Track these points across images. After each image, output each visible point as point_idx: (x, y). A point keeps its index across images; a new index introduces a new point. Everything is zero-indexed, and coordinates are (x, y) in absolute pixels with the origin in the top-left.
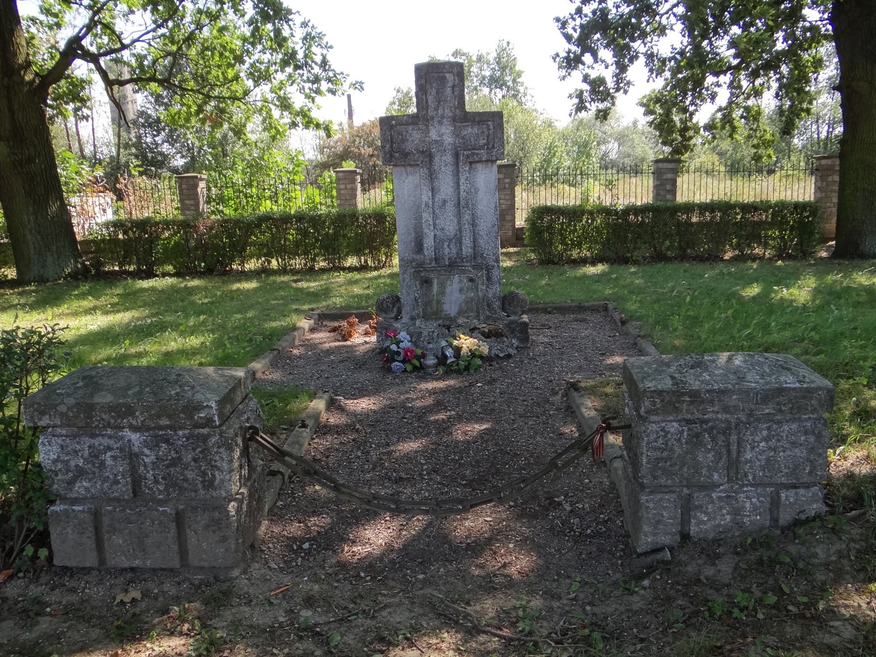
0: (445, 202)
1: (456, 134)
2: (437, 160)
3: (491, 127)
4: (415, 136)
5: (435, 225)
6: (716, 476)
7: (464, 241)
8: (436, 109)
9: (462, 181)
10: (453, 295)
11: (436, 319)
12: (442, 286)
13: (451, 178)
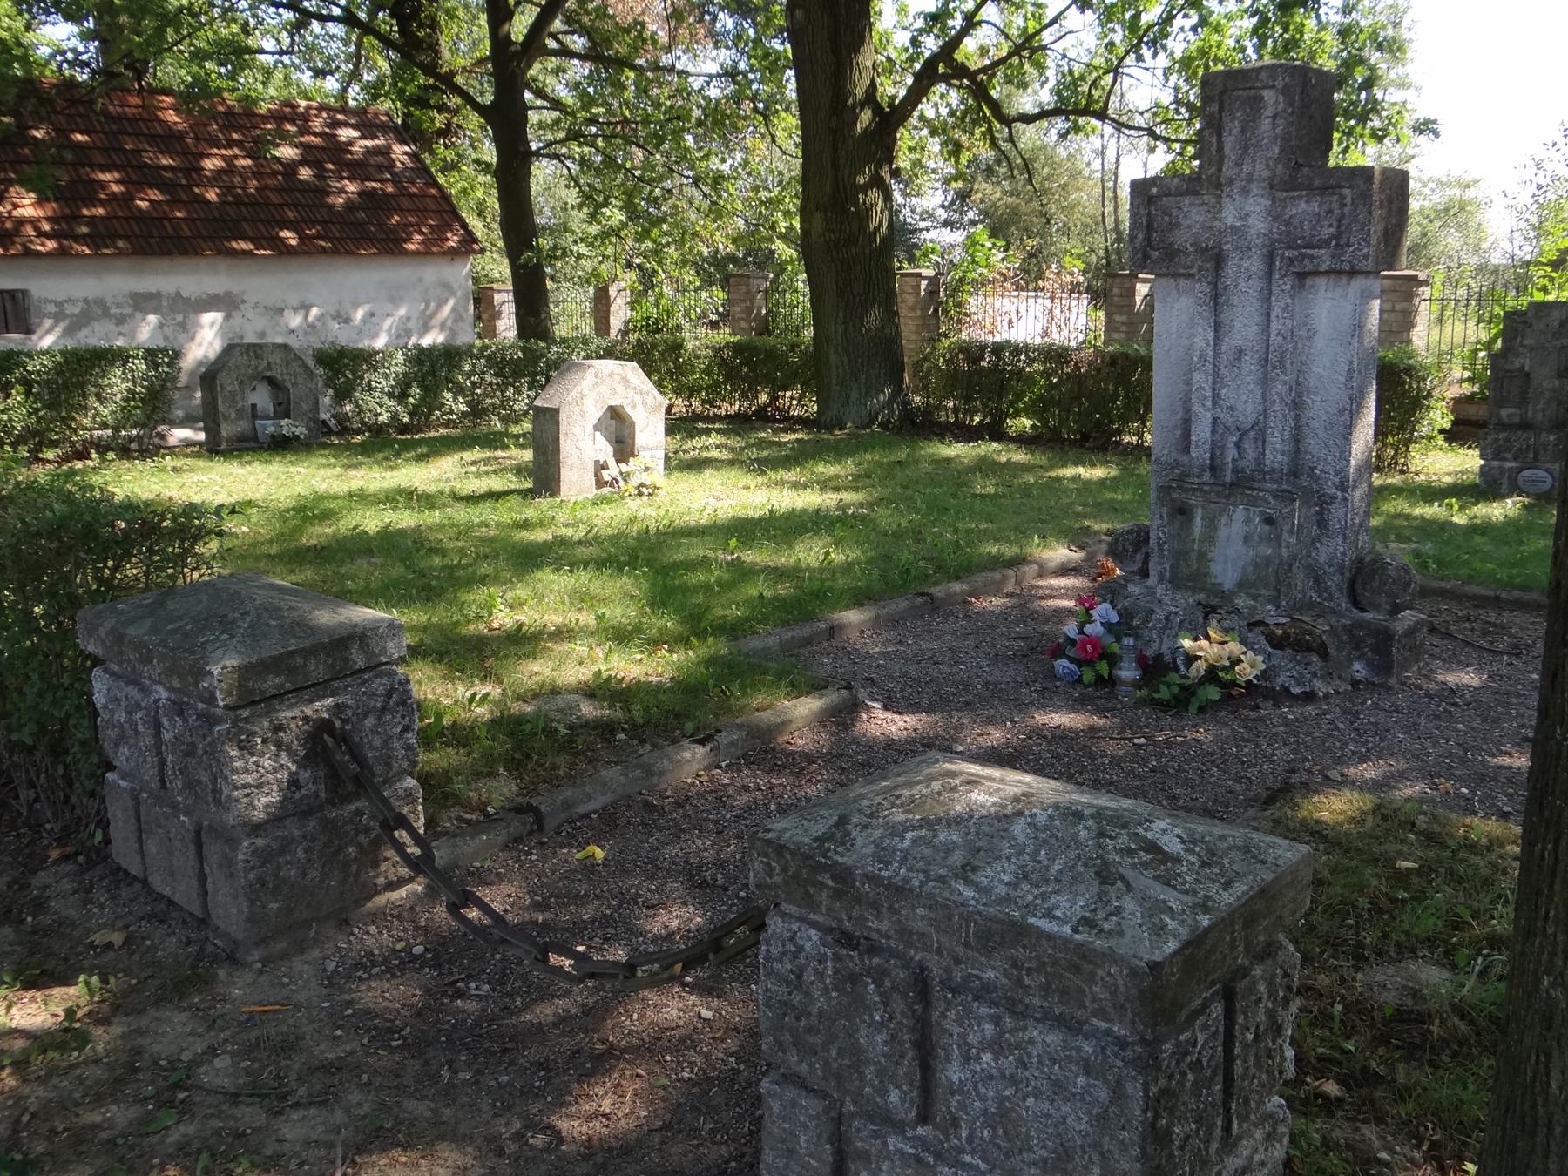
0: (1240, 353)
1: (1275, 215)
2: (1230, 268)
3: (1348, 200)
4: (1193, 218)
5: (1216, 399)
6: (894, 1097)
7: (1269, 438)
8: (1239, 164)
9: (1276, 311)
10: (1232, 544)
11: (1194, 591)
12: (1211, 523)
13: (1257, 304)
